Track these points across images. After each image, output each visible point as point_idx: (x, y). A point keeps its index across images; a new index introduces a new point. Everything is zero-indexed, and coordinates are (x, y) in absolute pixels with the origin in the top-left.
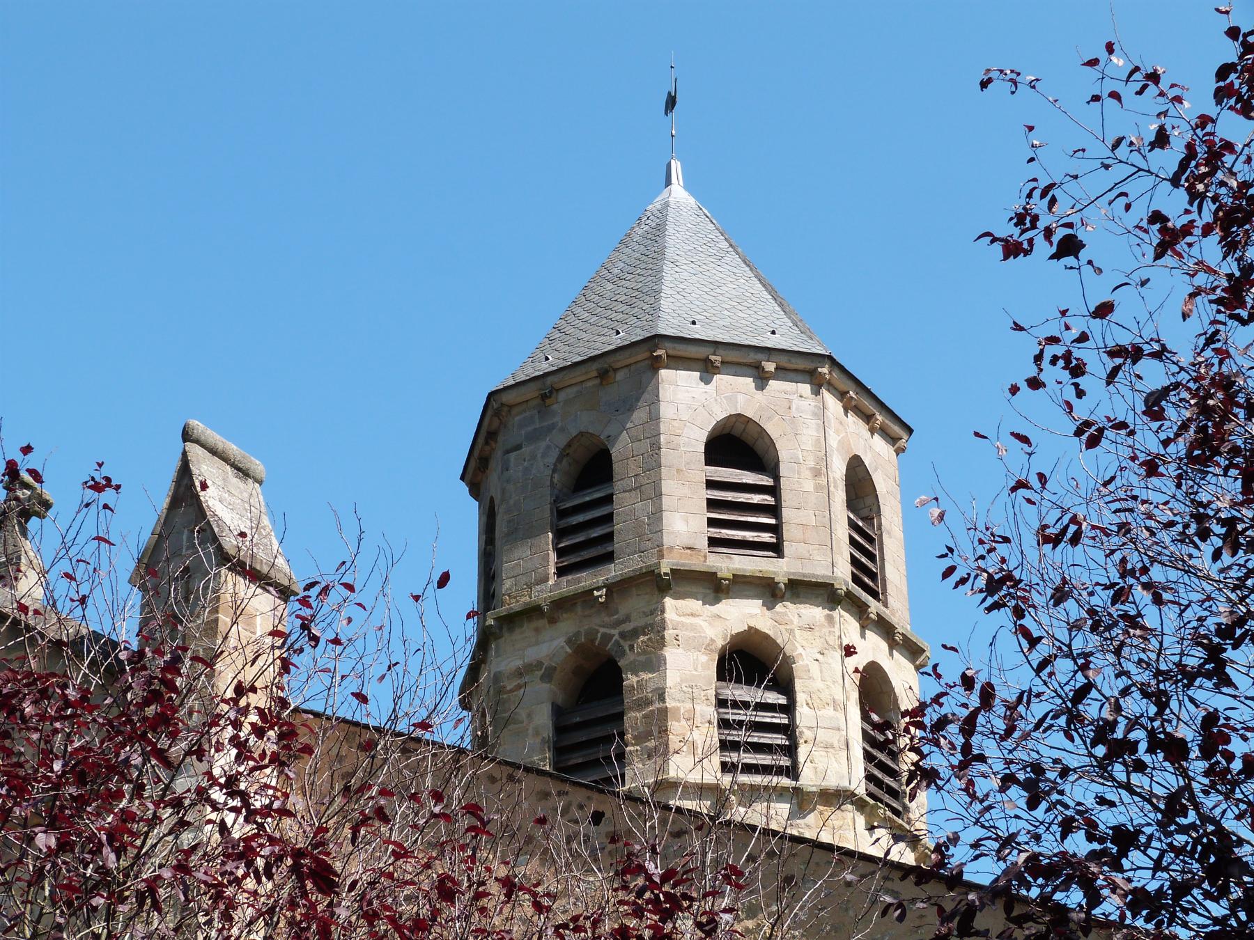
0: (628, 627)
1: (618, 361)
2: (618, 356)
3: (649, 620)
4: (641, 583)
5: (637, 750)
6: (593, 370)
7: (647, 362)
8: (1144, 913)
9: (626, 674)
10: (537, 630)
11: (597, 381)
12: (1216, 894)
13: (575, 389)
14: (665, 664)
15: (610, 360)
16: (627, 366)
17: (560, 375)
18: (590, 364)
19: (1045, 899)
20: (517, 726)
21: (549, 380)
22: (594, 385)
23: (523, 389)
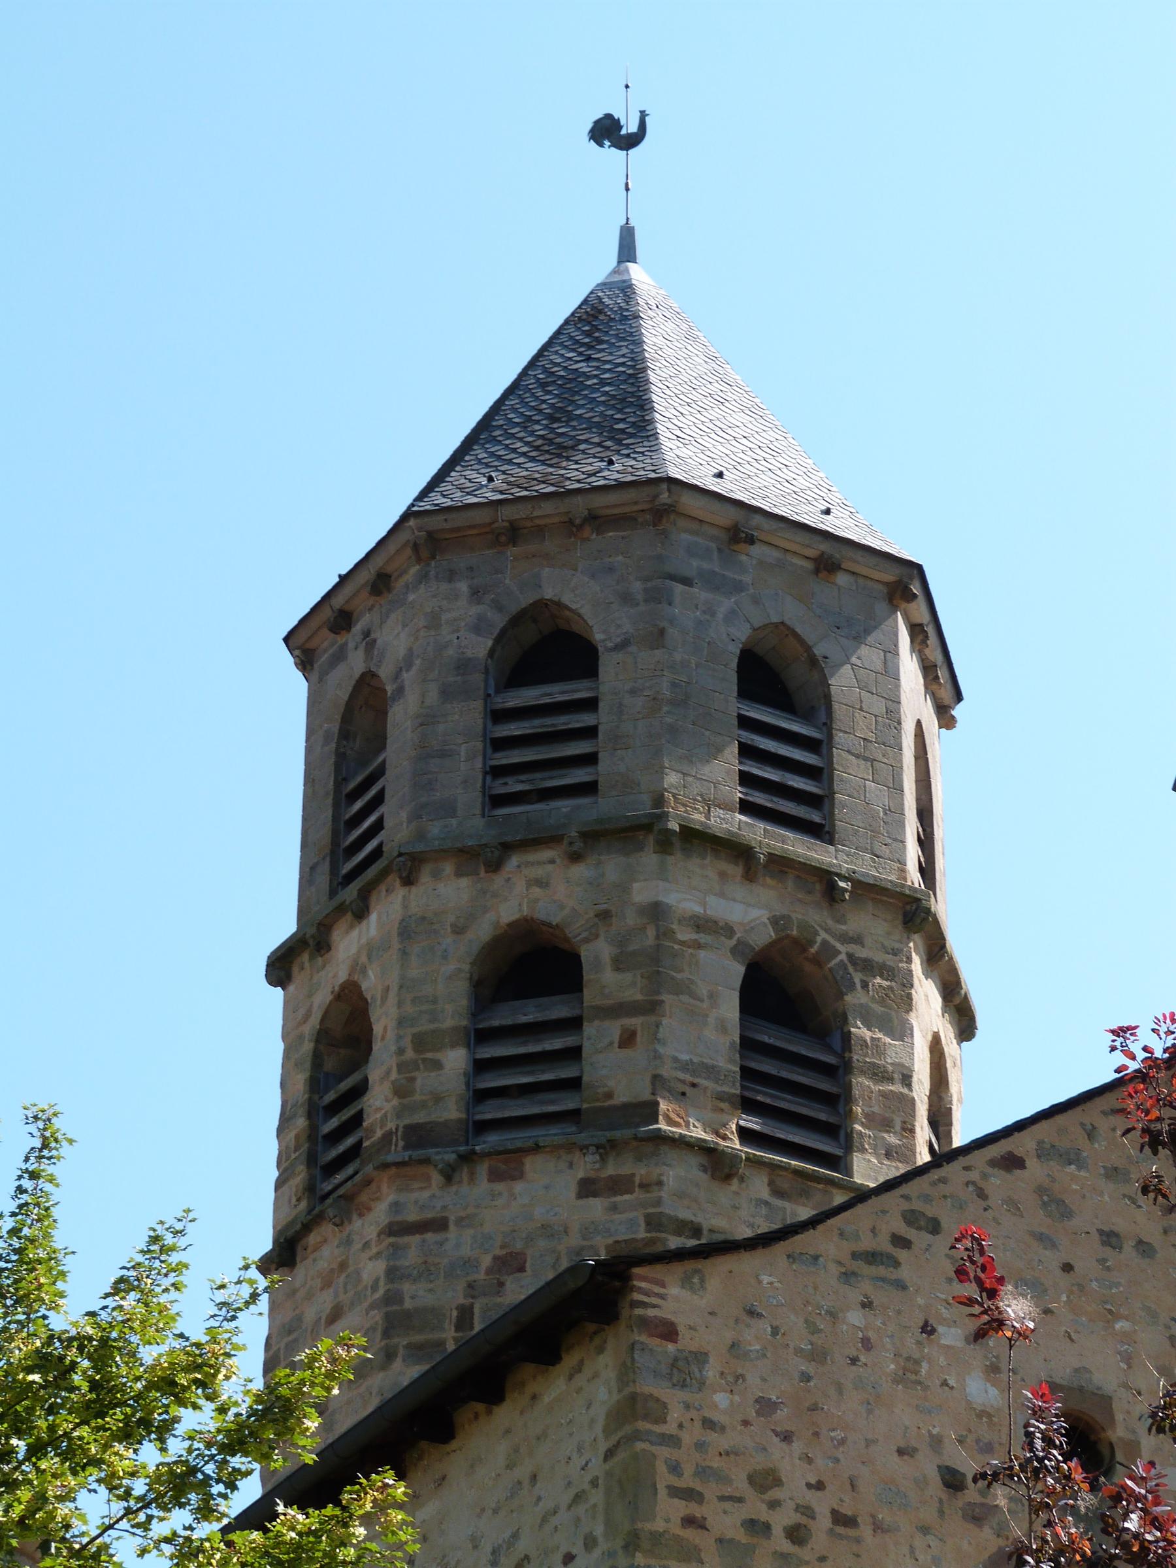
0: (862, 953)
1: (855, 561)
2: (859, 555)
3: (889, 960)
4: (881, 901)
5: (870, 1136)
6: (889, 575)
7: (881, 587)
8: (408, 1491)
9: (855, 1018)
10: (722, 875)
11: (809, 565)
12: (49, 1449)
13: (776, 554)
14: (912, 1036)
15: (849, 552)
16: (853, 573)
17: (774, 525)
18: (819, 538)
19: (24, 1378)
20: (692, 1001)
21: (757, 519)
22: (802, 566)
23: (717, 506)
